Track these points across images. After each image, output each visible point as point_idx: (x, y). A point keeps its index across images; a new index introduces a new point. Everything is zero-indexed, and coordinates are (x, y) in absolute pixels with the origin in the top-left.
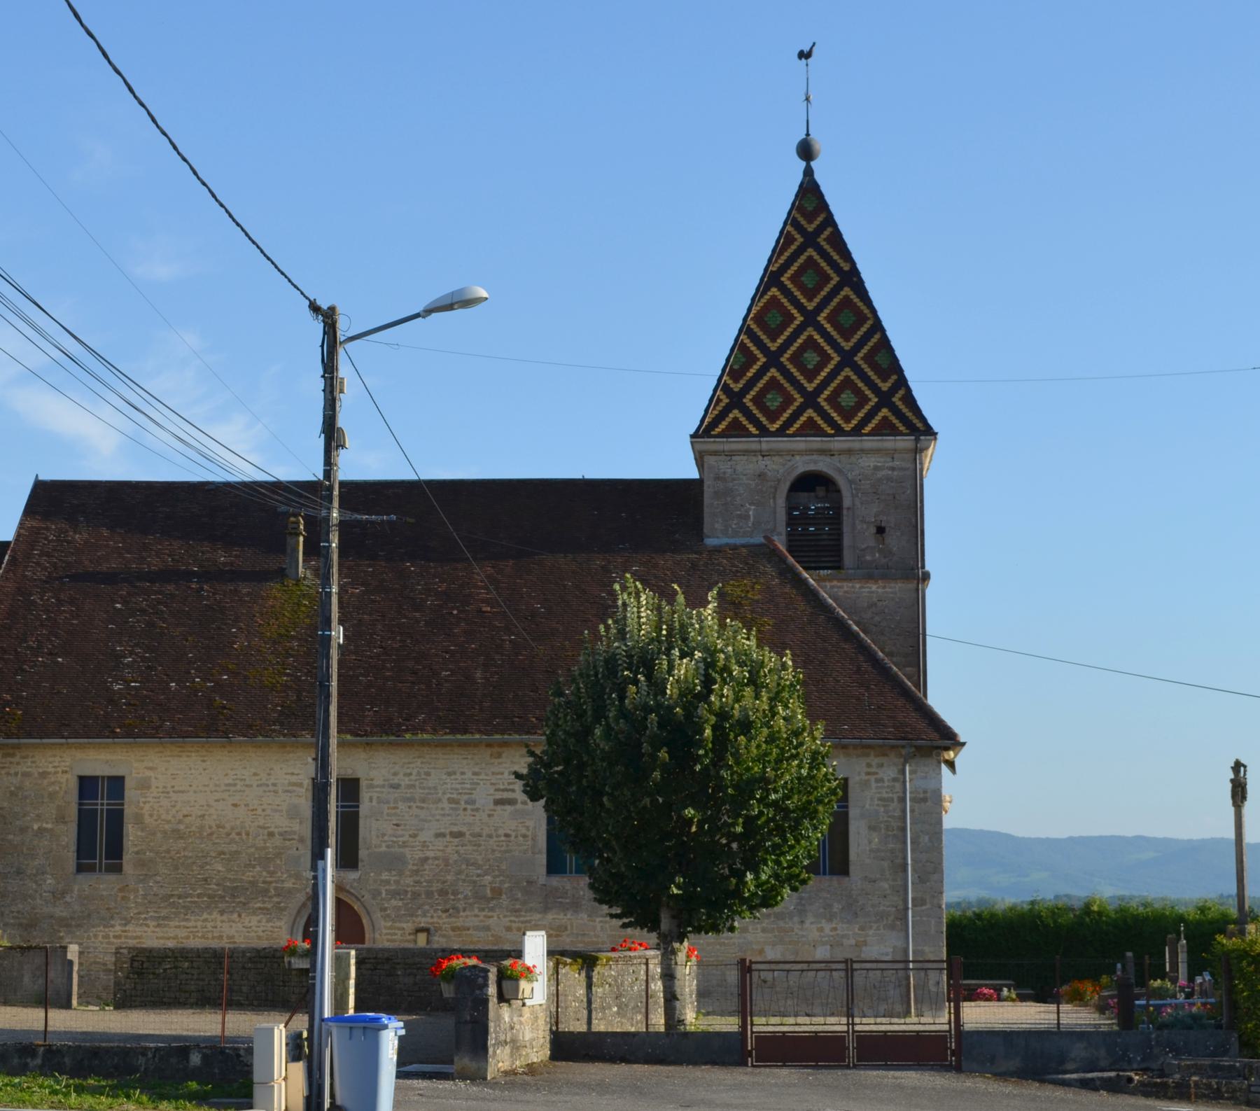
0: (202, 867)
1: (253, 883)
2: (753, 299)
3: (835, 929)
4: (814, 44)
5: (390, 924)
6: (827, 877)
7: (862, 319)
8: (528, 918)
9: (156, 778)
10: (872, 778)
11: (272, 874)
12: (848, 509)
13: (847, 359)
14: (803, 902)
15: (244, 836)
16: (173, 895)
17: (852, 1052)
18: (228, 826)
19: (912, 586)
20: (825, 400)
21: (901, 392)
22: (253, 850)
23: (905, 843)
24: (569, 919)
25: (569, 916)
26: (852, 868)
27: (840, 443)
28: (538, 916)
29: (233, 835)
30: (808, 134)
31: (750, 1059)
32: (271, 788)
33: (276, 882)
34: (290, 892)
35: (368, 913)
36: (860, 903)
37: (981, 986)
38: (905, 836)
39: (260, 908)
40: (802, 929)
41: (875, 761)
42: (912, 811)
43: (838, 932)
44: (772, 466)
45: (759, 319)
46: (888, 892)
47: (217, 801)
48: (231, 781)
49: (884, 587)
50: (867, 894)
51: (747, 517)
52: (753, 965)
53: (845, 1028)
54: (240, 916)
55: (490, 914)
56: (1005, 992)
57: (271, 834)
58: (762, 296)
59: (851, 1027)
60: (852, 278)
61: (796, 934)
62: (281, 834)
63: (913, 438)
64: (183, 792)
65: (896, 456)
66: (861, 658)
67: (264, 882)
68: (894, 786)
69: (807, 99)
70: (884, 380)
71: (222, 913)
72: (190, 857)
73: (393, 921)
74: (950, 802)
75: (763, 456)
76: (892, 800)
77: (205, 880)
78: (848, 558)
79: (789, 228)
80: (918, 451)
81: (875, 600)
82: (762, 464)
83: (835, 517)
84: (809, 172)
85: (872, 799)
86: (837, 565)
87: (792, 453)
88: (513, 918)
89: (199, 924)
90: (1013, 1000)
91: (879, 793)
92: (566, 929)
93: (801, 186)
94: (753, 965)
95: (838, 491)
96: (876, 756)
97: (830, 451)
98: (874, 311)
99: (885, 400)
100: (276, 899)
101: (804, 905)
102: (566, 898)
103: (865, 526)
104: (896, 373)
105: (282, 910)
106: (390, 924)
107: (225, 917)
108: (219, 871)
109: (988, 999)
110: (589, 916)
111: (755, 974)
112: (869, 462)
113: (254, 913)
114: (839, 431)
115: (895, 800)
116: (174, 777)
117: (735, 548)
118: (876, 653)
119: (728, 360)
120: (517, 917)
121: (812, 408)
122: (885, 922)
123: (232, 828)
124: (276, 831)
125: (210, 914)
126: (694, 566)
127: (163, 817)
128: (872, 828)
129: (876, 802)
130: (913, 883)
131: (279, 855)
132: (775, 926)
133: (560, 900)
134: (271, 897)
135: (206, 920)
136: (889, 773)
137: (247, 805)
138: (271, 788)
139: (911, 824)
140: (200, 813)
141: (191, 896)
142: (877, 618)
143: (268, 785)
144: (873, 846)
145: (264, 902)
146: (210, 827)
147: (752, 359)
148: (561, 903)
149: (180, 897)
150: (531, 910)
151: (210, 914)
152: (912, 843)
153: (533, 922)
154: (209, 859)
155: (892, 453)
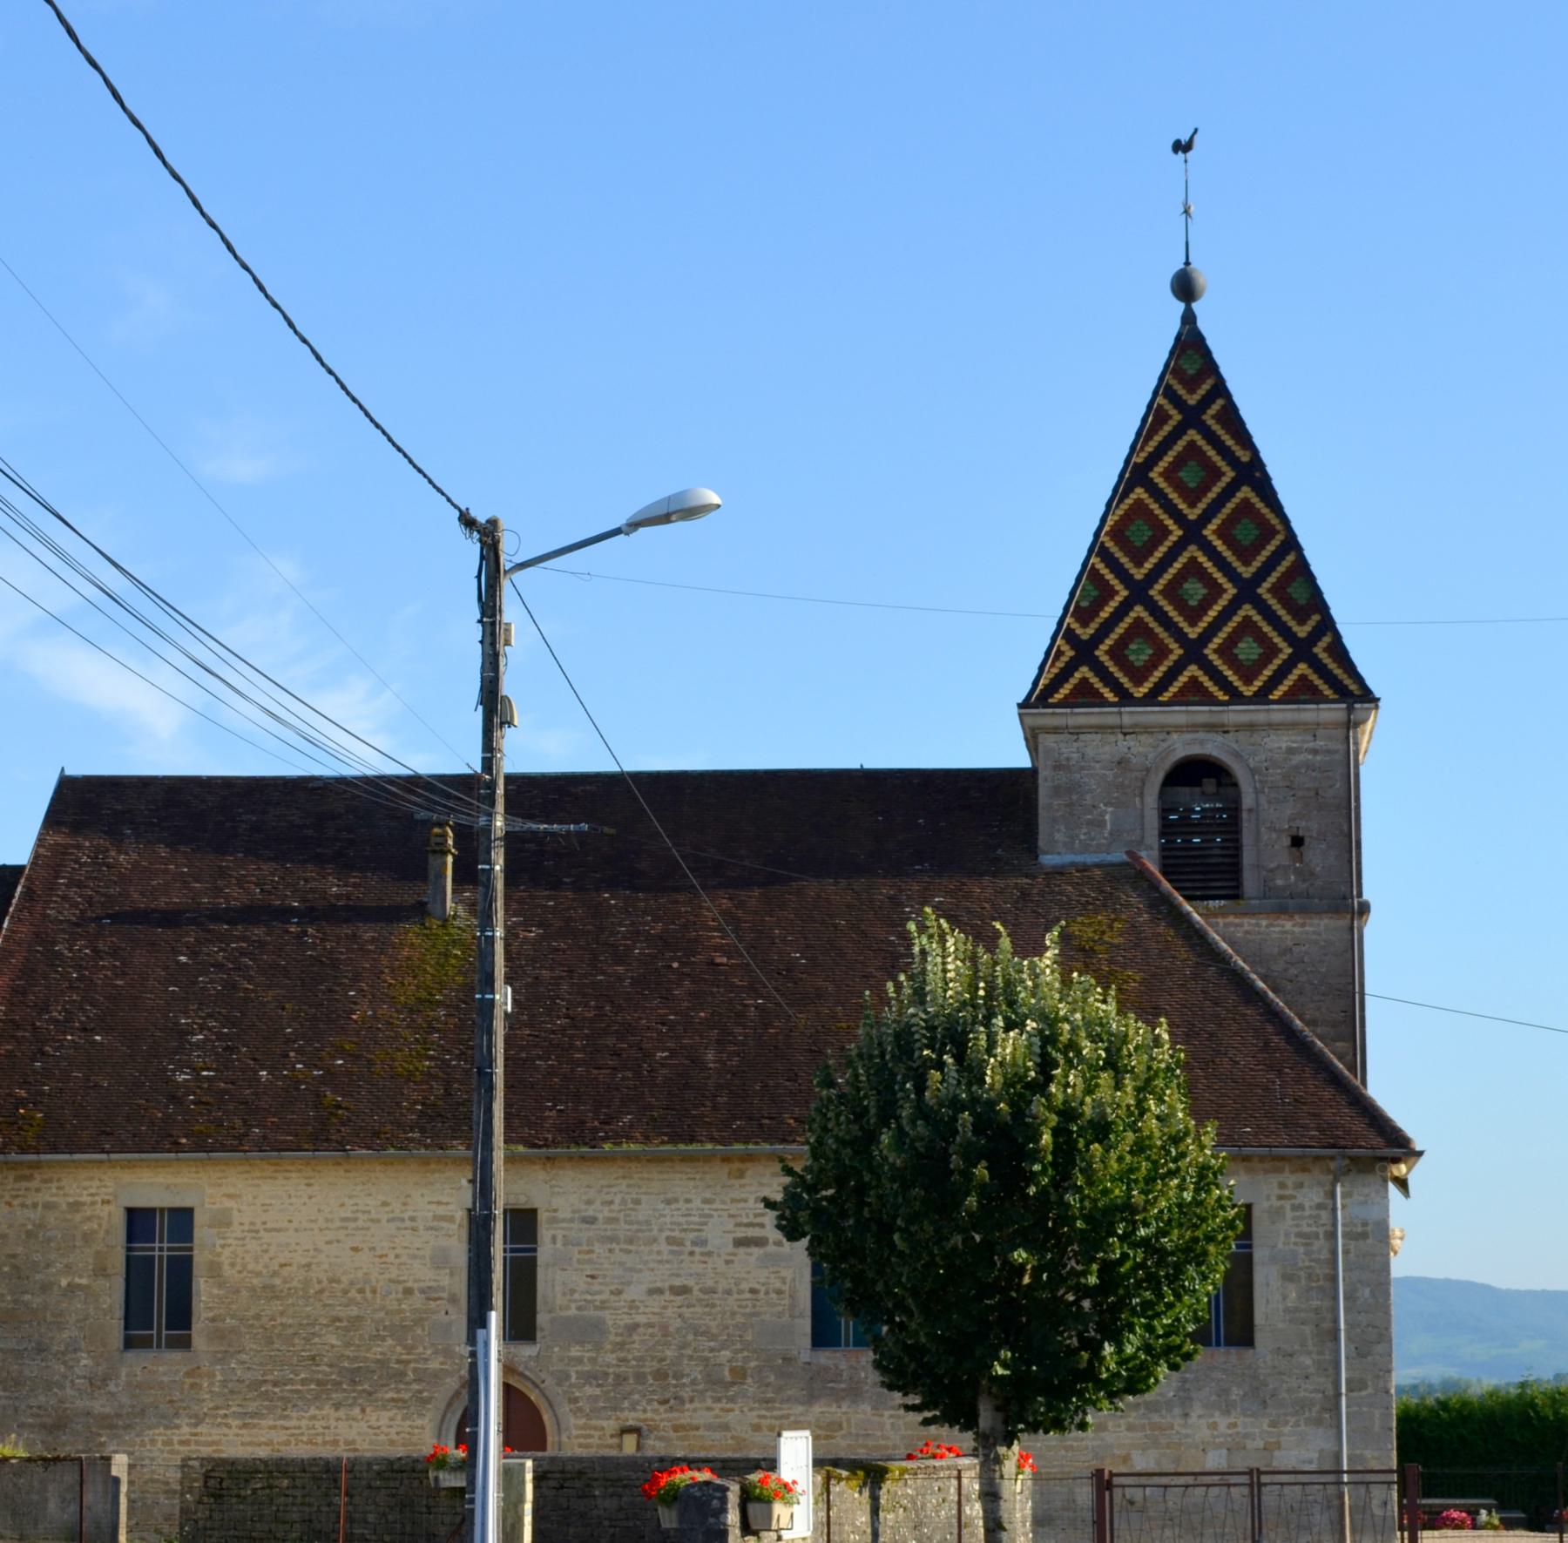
1: (382, 1363)
3: (1235, 1425)
4: (1196, 131)
6: (1222, 1349)
7: (1267, 533)
10: (1287, 1205)
11: (409, 1349)
12: (1250, 810)
14: (1187, 1386)
15: (369, 1295)
16: (265, 1381)
19: (1343, 922)
21: (1327, 639)
22: (382, 1314)
23: (1335, 1298)
24: (845, 1413)
26: (1259, 1337)
27: (1236, 714)
28: (800, 1409)
29: (353, 1293)
30: (1187, 263)
32: (408, 1224)
33: (416, 1361)
34: (437, 1376)
37: (1448, 1507)
39: (393, 1400)
40: (1185, 1426)
41: (1290, 1179)
42: (1346, 1252)
43: (1240, 1429)
44: (1139, 749)
45: (1118, 533)
46: (1312, 1370)
47: (328, 1243)
48: (349, 1215)
49: (1303, 925)
50: (1280, 1373)
51: (1102, 824)
54: (363, 1411)
55: (729, 1406)
56: (1483, 1516)
57: (408, 1292)
58: (1121, 501)
60: (1254, 473)
61: (1178, 1432)
62: (422, 1291)
63: (1344, 706)
66: (1270, 1028)
67: (399, 1362)
68: (1318, 1216)
69: (1186, 212)
71: (337, 1406)
74: (1401, 1238)
76: (1316, 1236)
77: (313, 1358)
78: (1250, 882)
80: (1351, 725)
81: (1290, 943)
82: (1123, 744)
83: (1230, 822)
84: (1189, 318)
85: (1287, 1235)
87: (1168, 730)
88: (764, 1412)
89: (304, 1423)
90: (1495, 1528)
91: (1297, 1226)
93: (1178, 338)
96: (1292, 1172)
97: (1223, 725)
99: (1302, 651)
100: (415, 1387)
102: (841, 1382)
103: (1274, 836)
107: (342, 1413)
108: (333, 1346)
109: (1458, 1525)
110: (874, 1408)
112: (1280, 742)
113: (384, 1408)
114: (1236, 697)
115: (1321, 1236)
116: (266, 1207)
117: (1084, 868)
118: (1292, 1021)
120: (768, 1409)
123: (352, 1283)
124: (416, 1286)
126: (1025, 895)
127: (250, 1267)
128: (1288, 1278)
129: (1293, 1239)
130: (1347, 1358)
131: (419, 1322)
133: (830, 1385)
135: (314, 1418)
136: (1311, 1196)
137: (372, 1249)
138: (408, 1224)
140: (304, 1261)
141: (291, 1382)
142: (1293, 971)
145: (399, 1391)
146: (319, 1282)
147: (1107, 593)
148: (832, 1388)
149: (275, 1384)
150: (788, 1400)
152: (1346, 1298)
153: (792, 1418)
155: (1313, 729)
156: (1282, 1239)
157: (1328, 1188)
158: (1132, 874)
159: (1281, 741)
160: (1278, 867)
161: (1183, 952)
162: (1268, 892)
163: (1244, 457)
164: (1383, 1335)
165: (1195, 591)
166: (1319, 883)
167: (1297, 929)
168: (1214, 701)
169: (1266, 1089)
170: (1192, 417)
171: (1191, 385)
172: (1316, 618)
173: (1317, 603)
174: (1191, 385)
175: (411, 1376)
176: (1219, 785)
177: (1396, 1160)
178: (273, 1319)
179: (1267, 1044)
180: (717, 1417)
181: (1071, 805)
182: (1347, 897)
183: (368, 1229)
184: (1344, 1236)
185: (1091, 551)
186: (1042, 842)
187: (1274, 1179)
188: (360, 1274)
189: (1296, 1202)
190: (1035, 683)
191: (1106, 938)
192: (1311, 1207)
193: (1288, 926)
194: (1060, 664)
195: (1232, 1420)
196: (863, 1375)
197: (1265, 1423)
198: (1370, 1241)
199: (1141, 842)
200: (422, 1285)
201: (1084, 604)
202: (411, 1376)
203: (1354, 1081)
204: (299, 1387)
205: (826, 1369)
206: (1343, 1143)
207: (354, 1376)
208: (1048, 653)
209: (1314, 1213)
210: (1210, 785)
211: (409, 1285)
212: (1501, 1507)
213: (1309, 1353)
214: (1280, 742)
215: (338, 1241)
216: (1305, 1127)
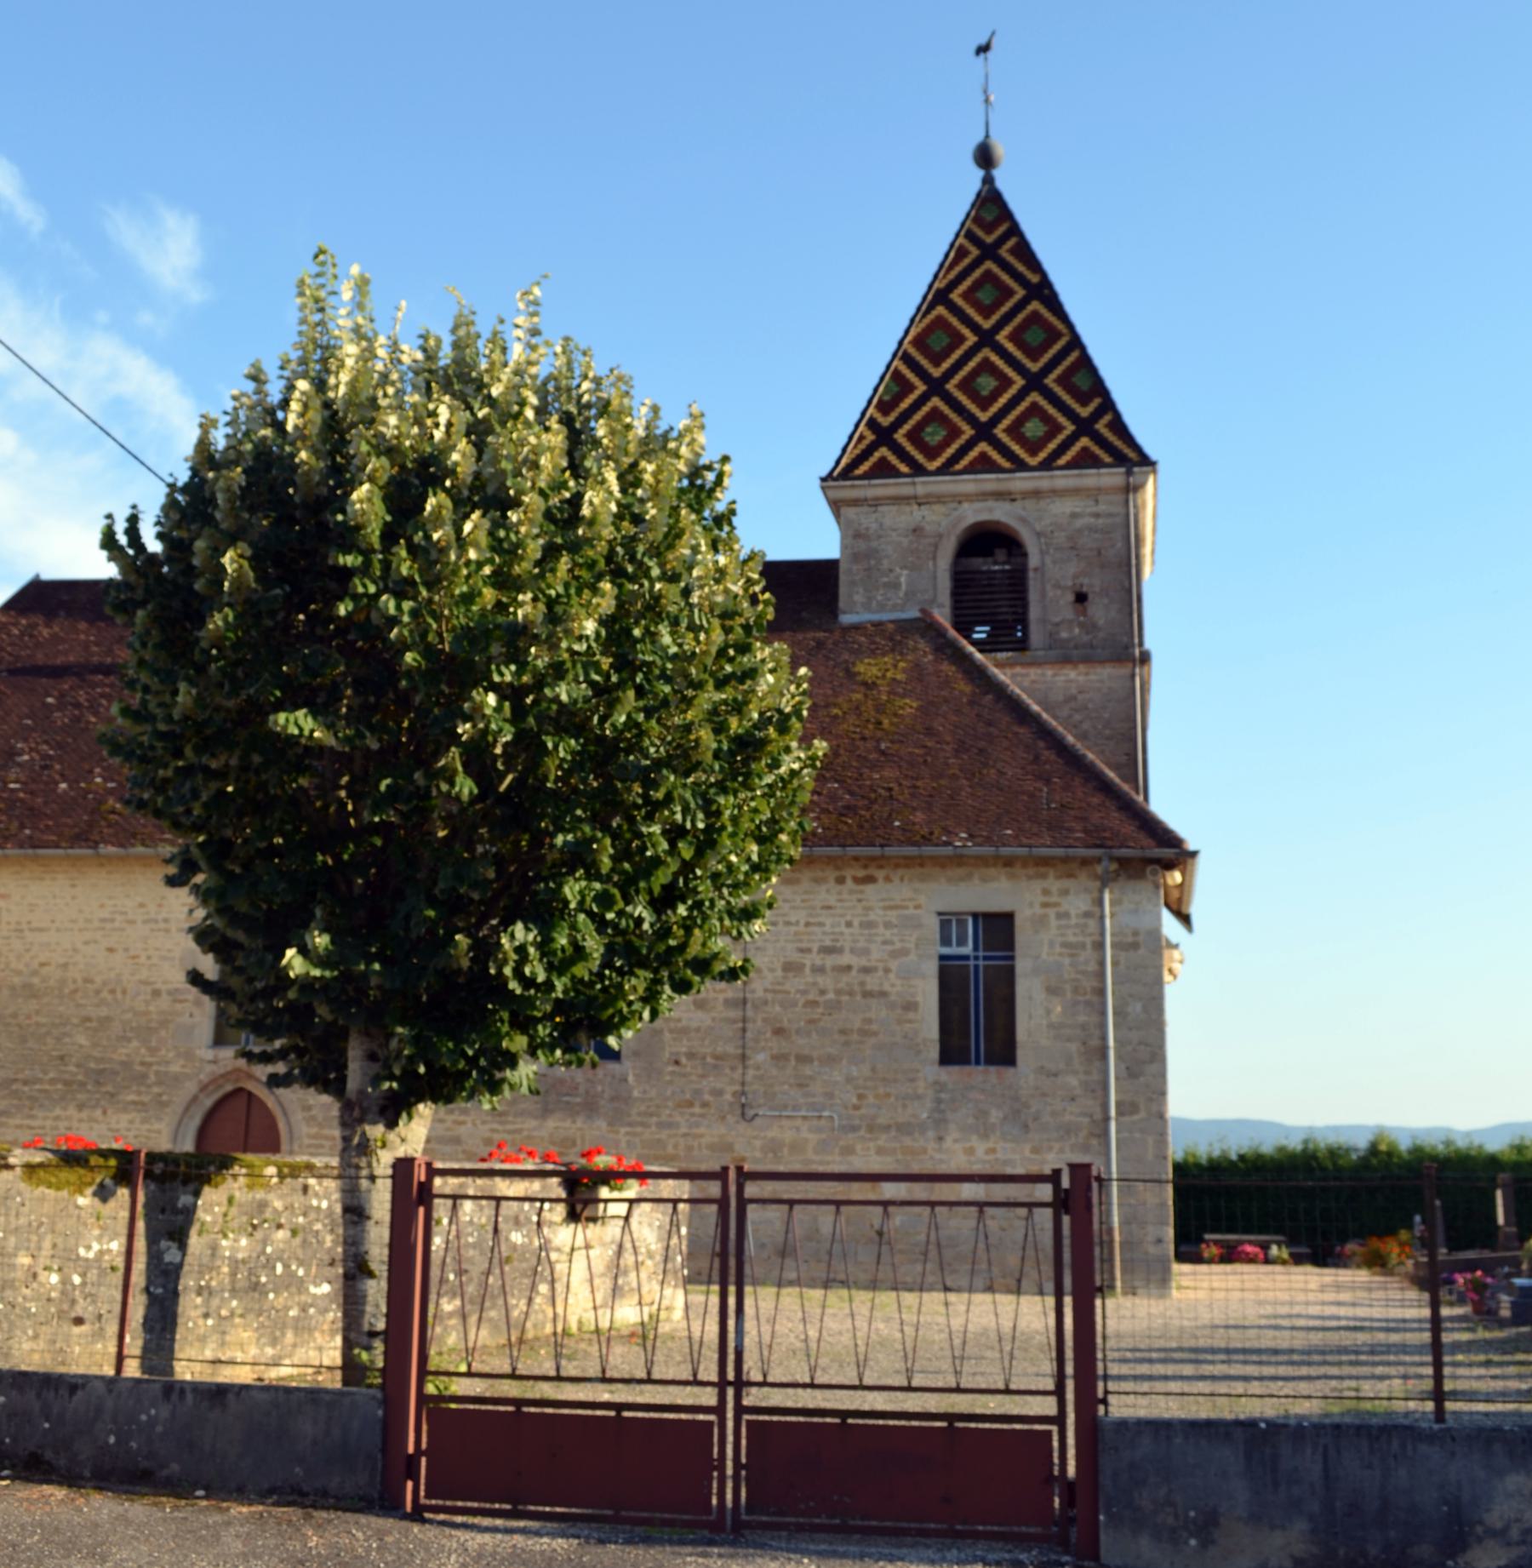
0: (58, 1039)
1: (126, 1065)
2: (912, 321)
3: (992, 1151)
4: (993, 34)
5: (314, 1130)
6: (981, 1068)
7: (1054, 335)
8: (518, 1126)
9: (8, 910)
10: (1051, 912)
11: (153, 1051)
12: (1036, 570)
13: (1034, 382)
14: (943, 1106)
15: (119, 995)
16: (16, 1080)
17: (728, 1493)
18: (98, 980)
19: (1124, 671)
20: (1005, 431)
21: (1108, 418)
22: (129, 1016)
23: (1103, 1013)
24: (580, 1129)
25: (579, 1124)
26: (1020, 1054)
27: (1021, 482)
28: (533, 1123)
29: (105, 994)
30: (987, 136)
31: (410, 1484)
32: (162, 925)
33: (159, 1063)
34: (177, 1079)
35: (285, 1113)
36: (1033, 1110)
37: (1242, 1243)
38: (1104, 1004)
39: (134, 1103)
40: (940, 1150)
41: (1054, 884)
42: (1115, 964)
43: (999, 1155)
44: (933, 517)
45: (919, 342)
46: (1078, 1092)
47: (86, 943)
48: (107, 916)
49: (1087, 674)
50: (1044, 1095)
51: (896, 586)
52: (438, 1181)
53: (708, 1397)
54: (105, 1112)
55: (462, 1118)
56: (1274, 1250)
57: (156, 993)
58: (924, 316)
59: (730, 1392)
60: (1044, 291)
61: (932, 1158)
62: (170, 993)
63: (1122, 470)
64: (41, 930)
65: (1101, 498)
66: (1041, 744)
67: (143, 1064)
68: (1086, 925)
69: (987, 101)
70: (1084, 404)
71: (81, 1107)
72: (44, 1025)
73: (321, 1126)
74: (1181, 962)
75: (920, 504)
76: (1083, 946)
77: (62, 1058)
78: (1036, 636)
79: (961, 240)
80: (1131, 489)
81: (1074, 691)
82: (916, 514)
83: (1017, 582)
84: (988, 180)
85: (1051, 944)
86: (1022, 645)
87: (959, 499)
88: (496, 1126)
89: (49, 1123)
90: (1284, 1263)
91: (1062, 935)
92: (574, 1144)
93: (979, 195)
94: (438, 1181)
95: (1025, 555)
96: (1058, 877)
97: (1010, 493)
98: (1071, 327)
99: (1085, 427)
100: (156, 1090)
101: (943, 1111)
102: (576, 1095)
103: (1059, 592)
104: (1100, 395)
105: (163, 1105)
106: (314, 1130)
107: (84, 1114)
108: (81, 1046)
109: (1251, 1260)
110: (610, 1124)
111: (441, 1208)
112: (1063, 508)
113: (125, 1110)
114: (1021, 466)
115: (1089, 946)
116: (32, 908)
117: (878, 625)
118: (1064, 738)
119: (876, 390)
120: (501, 1123)
121: (985, 440)
122: (1073, 1140)
123: (105, 983)
124: (164, 988)
125: (65, 1109)
126: (820, 644)
127: (13, 965)
128: (1052, 991)
129: (1058, 949)
130: (1117, 1078)
131: (164, 1024)
132: (898, 1145)
133: (566, 1099)
134: (149, 1086)
135: (57, 1118)
136: (1078, 903)
137: (126, 950)
138: (162, 925)
139: (1113, 983)
140: (62, 961)
141: (39, 1081)
142: (1077, 717)
143: (156, 921)
144: (1054, 1018)
145: (139, 1093)
146: (75, 981)
147: (908, 388)
148: (568, 1103)
149: (25, 1083)
150: (522, 1113)
151: (65, 1109)
152: (1115, 1013)
153: (525, 1133)
154: (68, 1028)
155: (1095, 494)
156: (1046, 949)
157: (1096, 894)
158: (926, 626)
159: (1064, 507)
160: (1062, 622)
161: (964, 687)
162: (1053, 642)
163: (1034, 279)
164: (1157, 1055)
165: (987, 383)
166: (1101, 635)
167: (1081, 678)
168: (1001, 470)
169: (1031, 796)
170: (989, 252)
171: (989, 229)
172: (1097, 402)
173: (1099, 389)
174: (989, 229)
175: (152, 1078)
176: (1010, 554)
177: (1169, 866)
178: (29, 1017)
179: (1037, 758)
180: (448, 1129)
181: (869, 569)
182: (1129, 646)
183: (123, 930)
184: (1114, 945)
185: (895, 355)
186: (842, 604)
187: (1037, 885)
188: (112, 975)
189: (1062, 909)
190: (838, 462)
191: (889, 675)
192: (1077, 916)
193: (1073, 676)
194: (862, 446)
195: (991, 1145)
196: (599, 1088)
197: (1027, 1148)
198: (1142, 951)
199: (933, 601)
200: (170, 986)
201: (887, 398)
202: (152, 1078)
203: (1133, 794)
204: (47, 1087)
205: (562, 1081)
206: (1110, 843)
207: (99, 1077)
208: (851, 438)
209: (1082, 921)
210: (1001, 554)
211: (158, 986)
212: (1291, 1241)
213: (1075, 1073)
214: (1063, 508)
215: (96, 942)
216: (1070, 830)
